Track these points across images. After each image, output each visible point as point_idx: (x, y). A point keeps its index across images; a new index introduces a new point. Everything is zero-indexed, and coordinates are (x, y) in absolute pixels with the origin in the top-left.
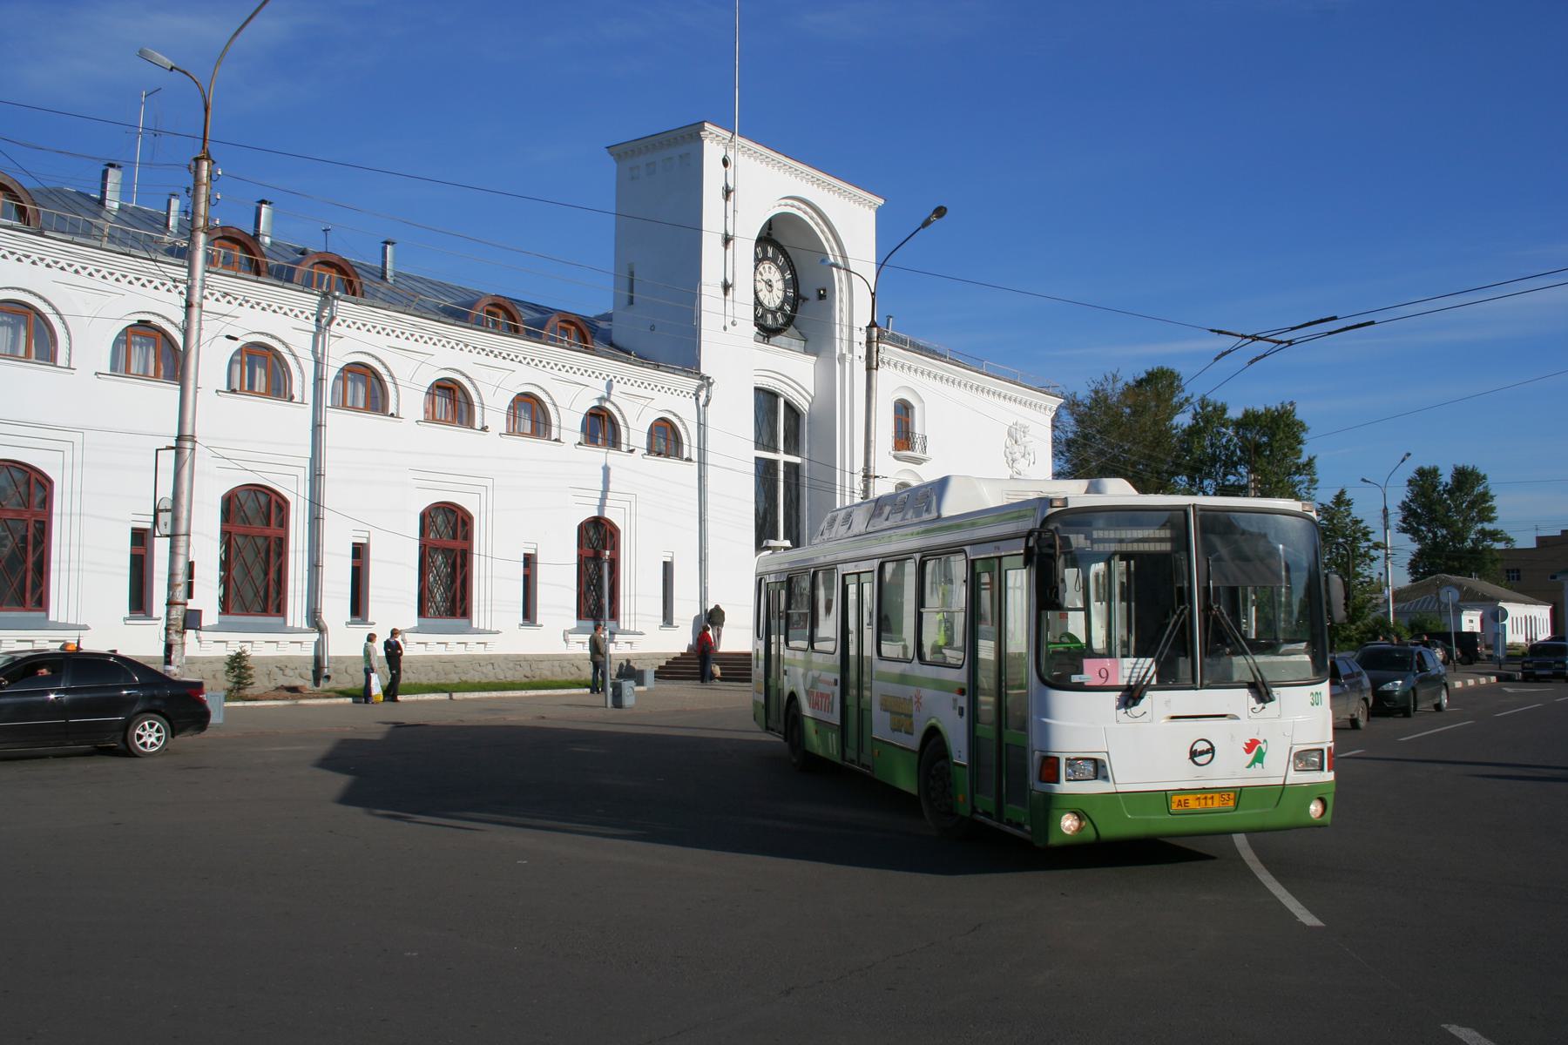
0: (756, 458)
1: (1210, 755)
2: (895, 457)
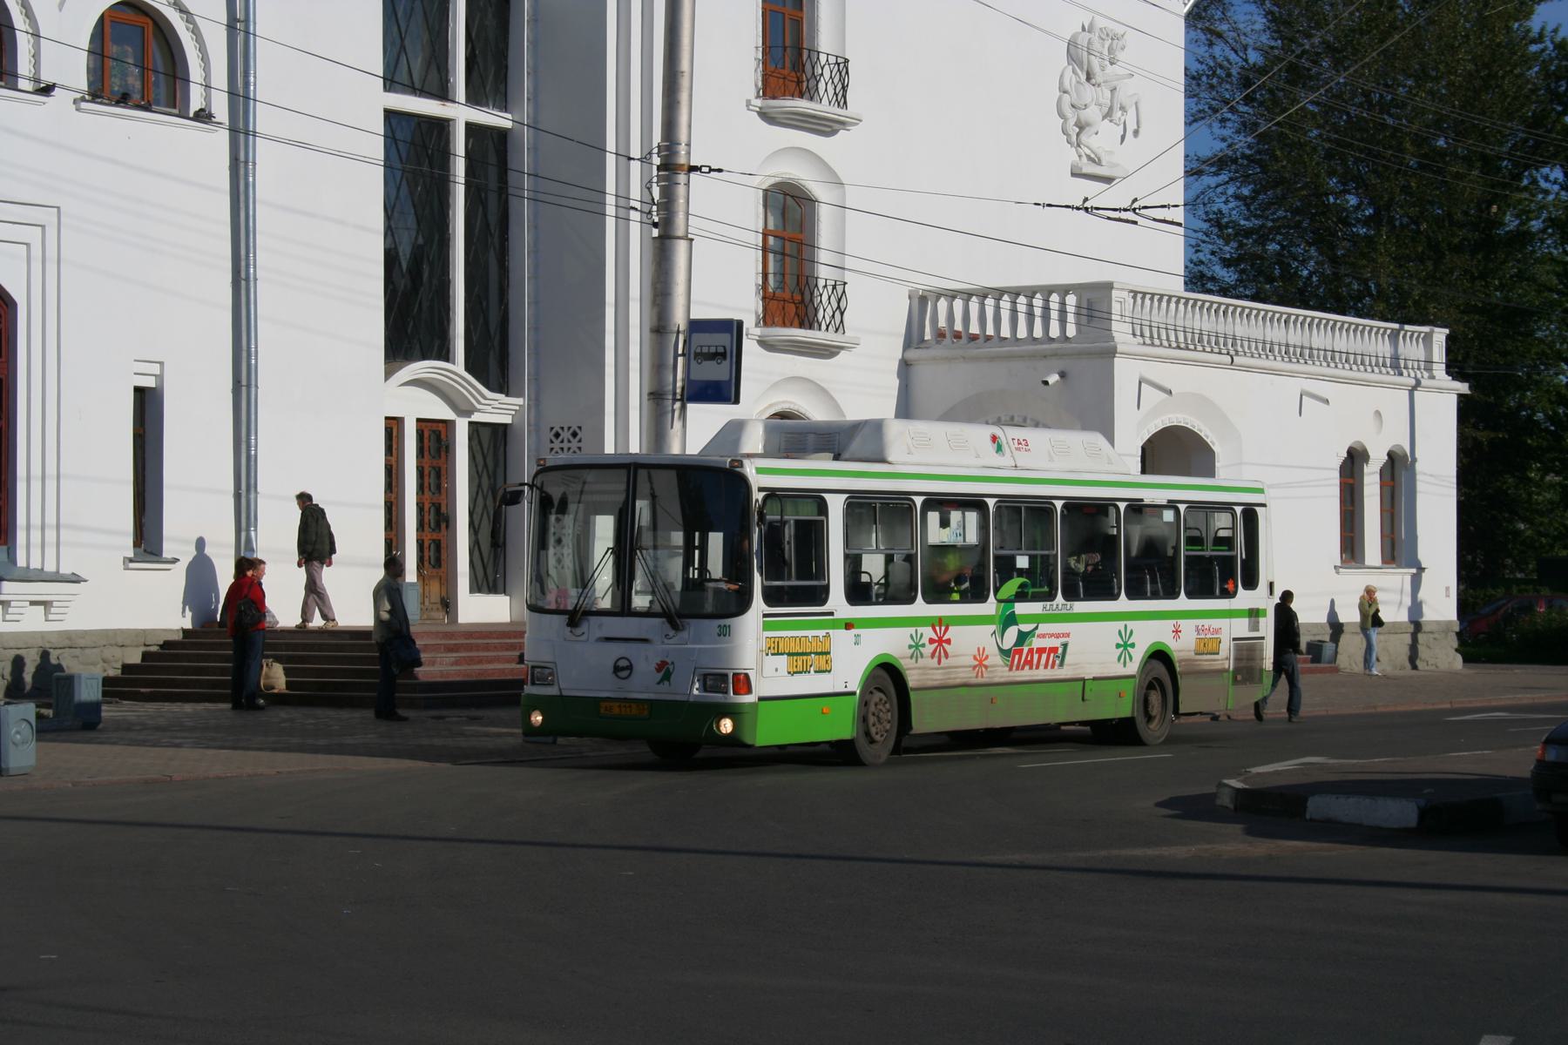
0: (390, 114)
1: (629, 671)
2: (765, 116)
